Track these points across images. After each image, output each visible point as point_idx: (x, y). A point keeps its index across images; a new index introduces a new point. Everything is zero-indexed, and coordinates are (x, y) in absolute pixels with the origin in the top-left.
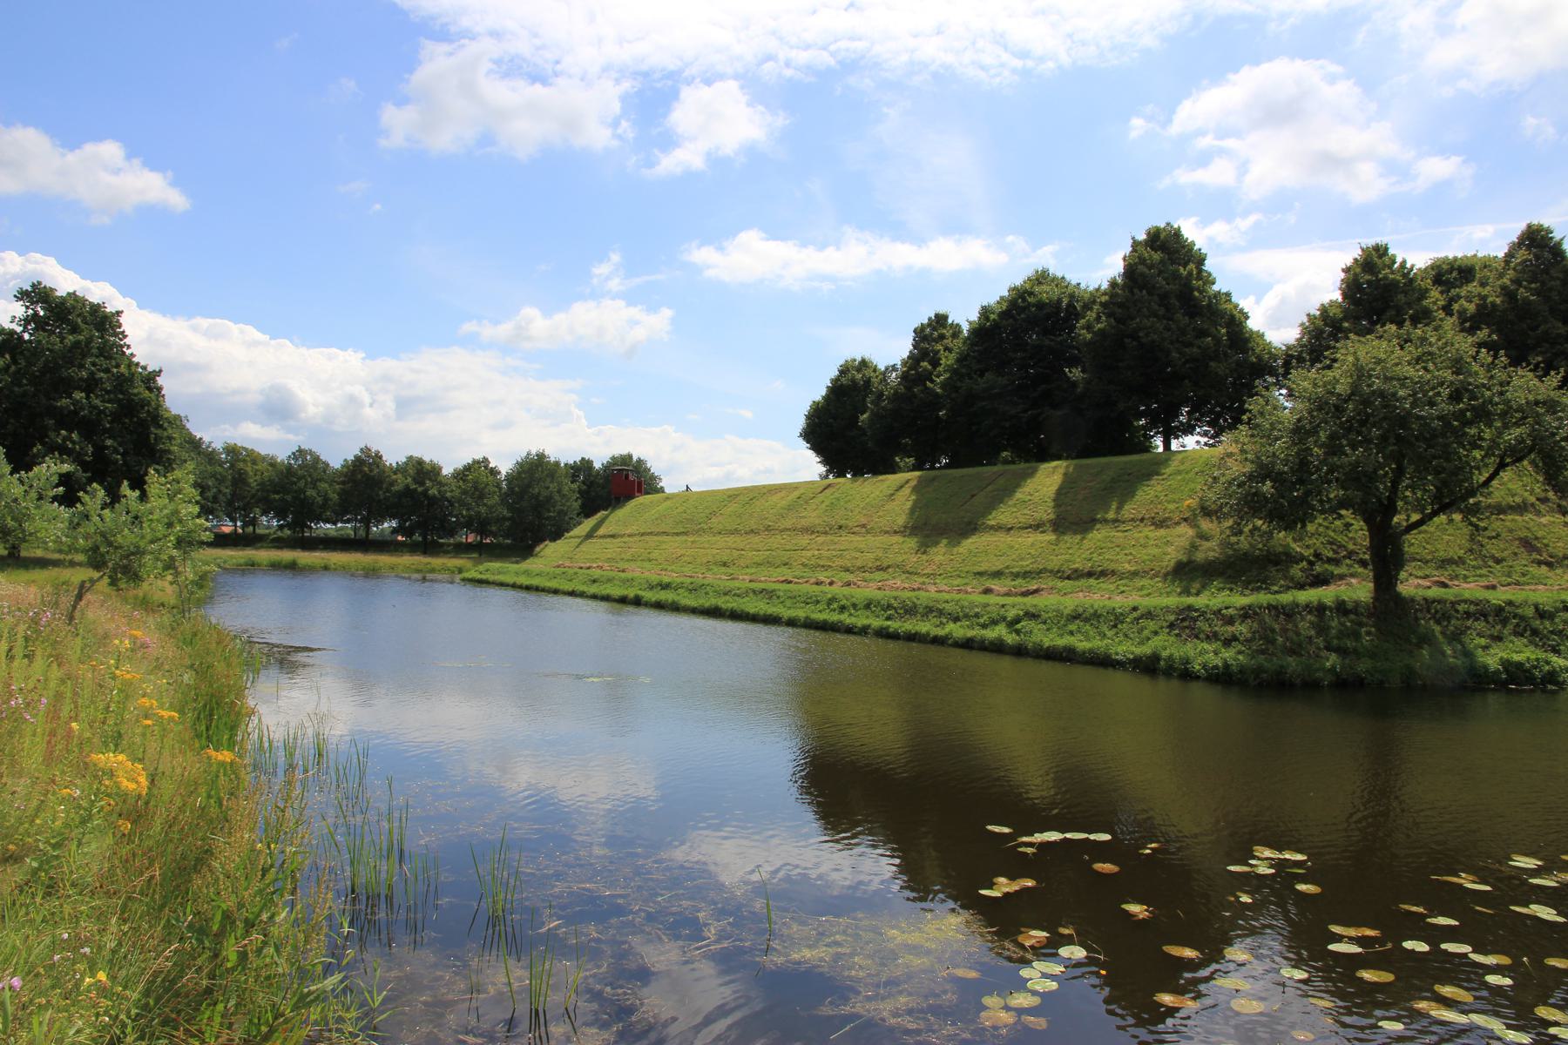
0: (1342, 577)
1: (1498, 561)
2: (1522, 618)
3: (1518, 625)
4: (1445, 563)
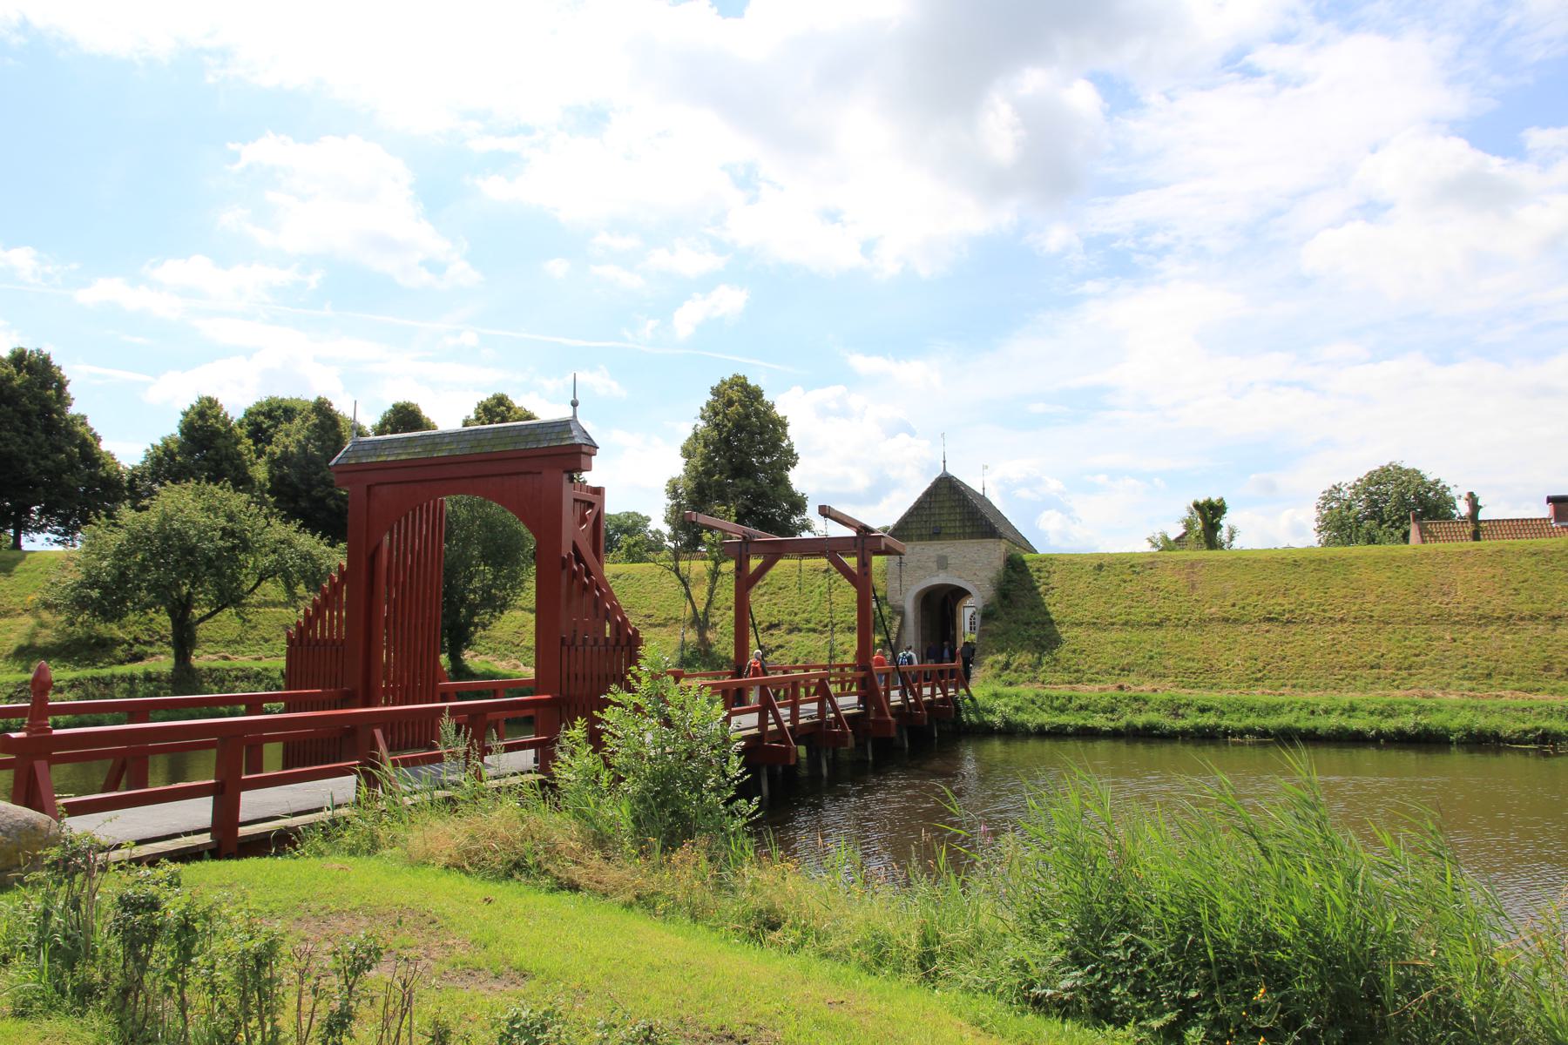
0: (153, 655)
1: (267, 641)
2: (272, 679)
3: (268, 683)
4: (229, 643)
